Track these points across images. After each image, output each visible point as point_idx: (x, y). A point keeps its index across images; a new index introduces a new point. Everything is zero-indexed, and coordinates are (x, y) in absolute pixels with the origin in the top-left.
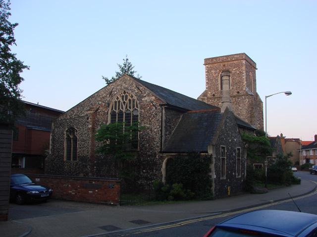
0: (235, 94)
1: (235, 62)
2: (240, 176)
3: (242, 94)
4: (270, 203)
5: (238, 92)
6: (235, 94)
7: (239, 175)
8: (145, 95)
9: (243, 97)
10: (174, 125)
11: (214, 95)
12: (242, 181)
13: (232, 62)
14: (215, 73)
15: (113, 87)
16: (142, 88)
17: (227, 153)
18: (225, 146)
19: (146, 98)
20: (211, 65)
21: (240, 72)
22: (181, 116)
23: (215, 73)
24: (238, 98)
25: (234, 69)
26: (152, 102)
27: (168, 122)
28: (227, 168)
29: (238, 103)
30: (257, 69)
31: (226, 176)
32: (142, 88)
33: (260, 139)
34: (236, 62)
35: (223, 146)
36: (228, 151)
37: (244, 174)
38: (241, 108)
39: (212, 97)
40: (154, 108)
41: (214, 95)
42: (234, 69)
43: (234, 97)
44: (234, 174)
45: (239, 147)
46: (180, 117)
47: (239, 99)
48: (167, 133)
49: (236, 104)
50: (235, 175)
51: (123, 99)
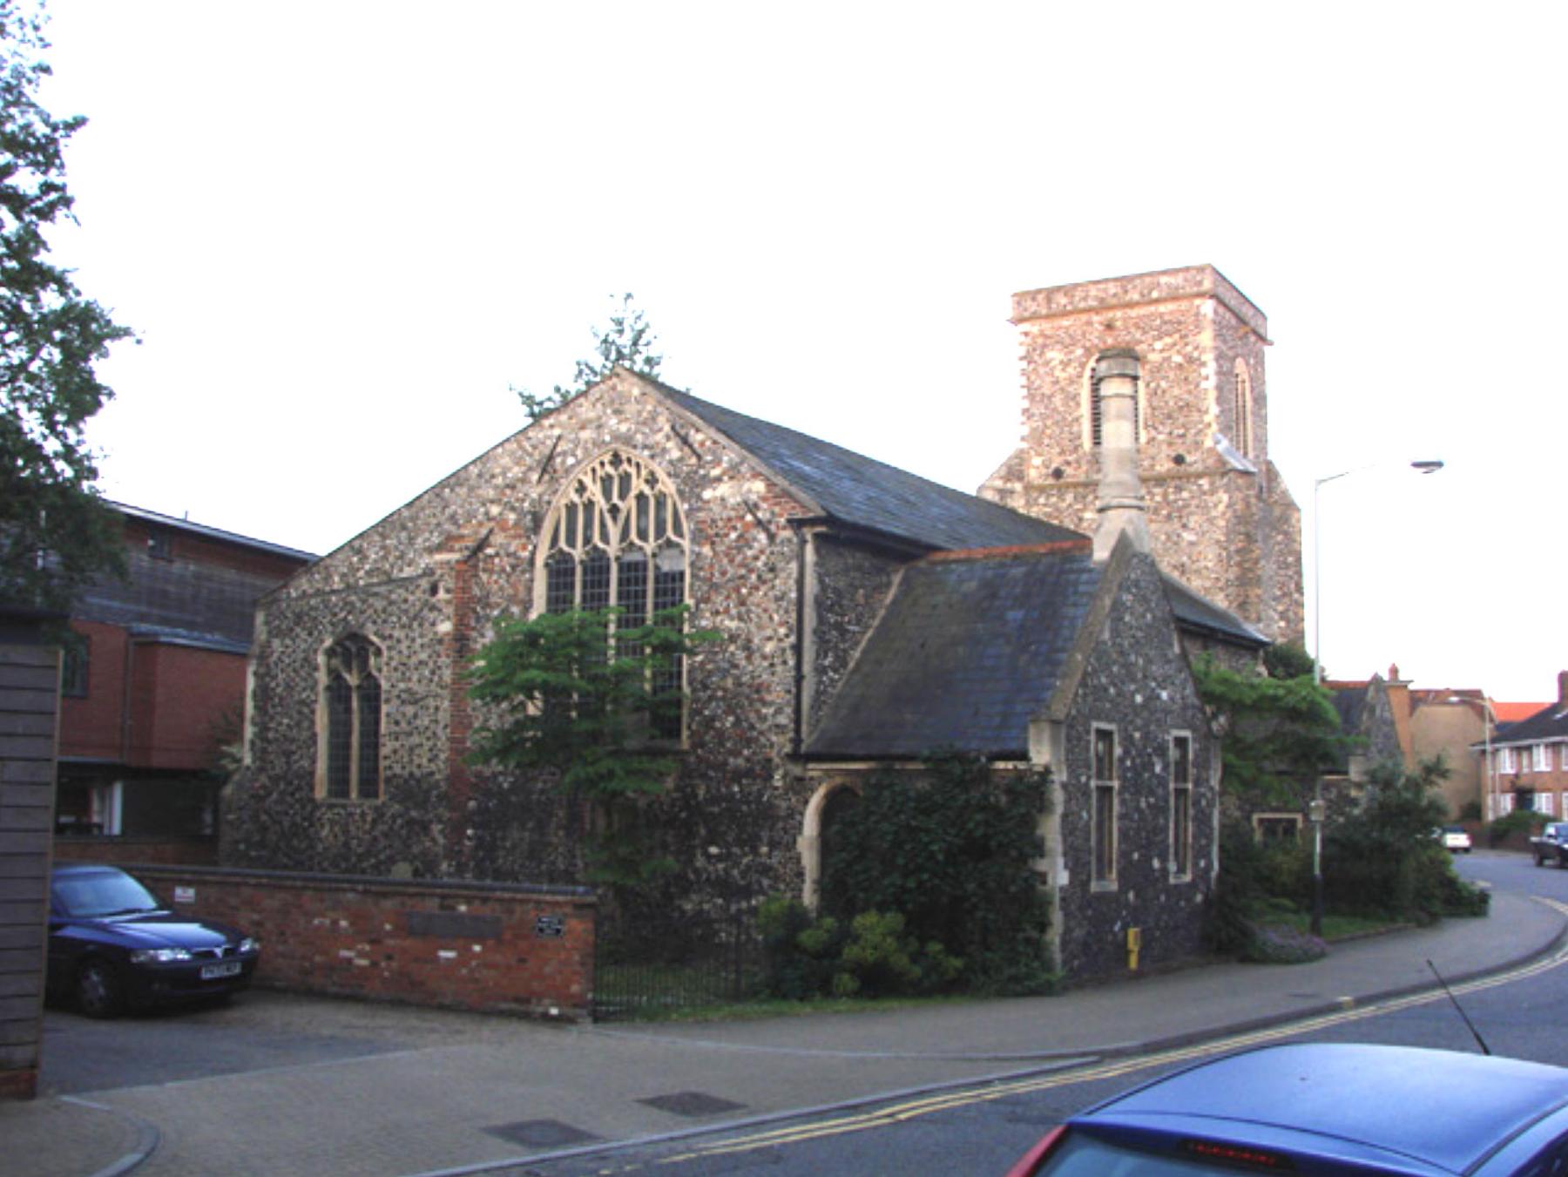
0: (1164, 466)
1: (1162, 308)
2: (1187, 878)
3: (1199, 467)
5: (1179, 460)
6: (1164, 466)
7: (1181, 870)
10: (858, 623)
11: (1058, 474)
17: (1122, 760)
22: (897, 579)
24: (1179, 489)
25: (1158, 345)
26: (753, 508)
28: (1124, 834)
29: (1177, 514)
32: (700, 437)
36: (1126, 752)
38: (1193, 538)
39: (1051, 481)
41: (1058, 474)
43: (1160, 481)
44: (1156, 864)
47: (1185, 495)
48: (826, 663)
49: (1169, 517)
50: (1164, 871)
51: (607, 493)
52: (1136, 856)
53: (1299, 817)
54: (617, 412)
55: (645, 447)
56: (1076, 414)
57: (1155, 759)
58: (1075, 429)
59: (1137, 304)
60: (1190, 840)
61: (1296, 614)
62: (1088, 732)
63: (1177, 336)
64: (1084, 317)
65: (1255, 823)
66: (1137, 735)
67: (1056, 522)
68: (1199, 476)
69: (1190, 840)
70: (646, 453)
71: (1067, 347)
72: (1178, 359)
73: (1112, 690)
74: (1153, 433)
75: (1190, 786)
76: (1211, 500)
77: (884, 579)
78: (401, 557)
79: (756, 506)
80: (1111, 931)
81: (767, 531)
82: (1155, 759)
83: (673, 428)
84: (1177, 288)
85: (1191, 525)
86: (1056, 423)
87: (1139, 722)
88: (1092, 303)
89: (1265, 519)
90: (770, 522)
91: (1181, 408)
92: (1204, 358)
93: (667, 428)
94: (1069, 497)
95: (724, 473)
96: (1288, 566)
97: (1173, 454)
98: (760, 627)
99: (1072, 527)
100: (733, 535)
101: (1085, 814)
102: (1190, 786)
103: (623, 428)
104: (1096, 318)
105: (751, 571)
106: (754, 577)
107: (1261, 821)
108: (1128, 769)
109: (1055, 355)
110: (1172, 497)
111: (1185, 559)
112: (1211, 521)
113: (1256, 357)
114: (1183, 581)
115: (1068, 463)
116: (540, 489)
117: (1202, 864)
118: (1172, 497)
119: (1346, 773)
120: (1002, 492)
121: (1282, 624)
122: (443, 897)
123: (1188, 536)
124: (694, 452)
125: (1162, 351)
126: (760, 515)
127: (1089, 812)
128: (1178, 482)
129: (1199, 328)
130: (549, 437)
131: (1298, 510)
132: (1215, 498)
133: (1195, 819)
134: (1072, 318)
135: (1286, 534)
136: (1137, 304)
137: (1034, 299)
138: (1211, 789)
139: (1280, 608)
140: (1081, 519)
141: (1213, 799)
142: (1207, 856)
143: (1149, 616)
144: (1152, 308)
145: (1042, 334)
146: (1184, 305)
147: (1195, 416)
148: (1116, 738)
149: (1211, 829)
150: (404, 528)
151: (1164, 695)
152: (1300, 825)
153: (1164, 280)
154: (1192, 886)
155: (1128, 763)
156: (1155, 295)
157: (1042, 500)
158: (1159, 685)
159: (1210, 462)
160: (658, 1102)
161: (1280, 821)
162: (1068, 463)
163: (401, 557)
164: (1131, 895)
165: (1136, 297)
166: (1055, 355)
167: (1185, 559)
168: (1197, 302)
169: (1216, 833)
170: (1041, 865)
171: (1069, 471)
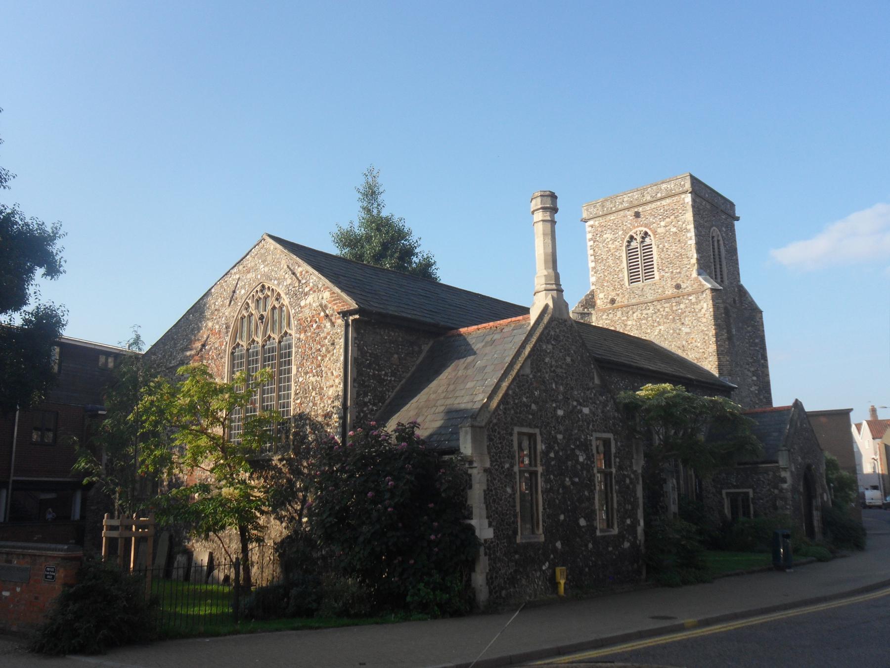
0: (670, 291)
1: (664, 202)
2: (615, 531)
3: (690, 289)
4: (681, 628)
5: (678, 287)
6: (670, 291)
7: (610, 525)
8: (307, 289)
9: (693, 298)
10: (393, 374)
11: (613, 301)
12: (627, 545)
13: (653, 205)
14: (614, 240)
15: (237, 276)
16: (300, 269)
17: (545, 454)
18: (537, 431)
19: (310, 299)
20: (601, 220)
21: (681, 230)
22: (426, 348)
23: (614, 240)
24: (679, 303)
25: (663, 224)
26: (323, 308)
27: (369, 366)
28: (549, 503)
29: (678, 318)
30: (738, 219)
31: (545, 532)
32: (300, 269)
33: (859, 426)
34: (668, 201)
35: (531, 431)
36: (550, 448)
37: (635, 523)
38: (688, 330)
39: (609, 306)
40: (328, 325)
41: (613, 301)
42: (663, 224)
43: (668, 299)
44: (582, 522)
45: (610, 436)
46: (420, 352)
47: (682, 306)
48: (366, 400)
49: (674, 320)
50: (592, 528)
51: (257, 307)
52: (562, 517)
53: (750, 491)
54: (264, 261)
55: (276, 279)
56: (621, 267)
57: (577, 452)
58: (620, 275)
59: (650, 202)
60: (615, 506)
61: (763, 372)
62: (511, 434)
63: (672, 217)
64: (622, 213)
65: (724, 496)
66: (560, 437)
67: (612, 328)
68: (689, 295)
69: (615, 506)
70: (276, 282)
71: (614, 231)
72: (674, 230)
73: (534, 407)
74: (663, 273)
75: (614, 470)
76: (698, 307)
77: (416, 349)
78: (171, 356)
79: (326, 306)
80: (541, 570)
81: (331, 320)
82: (577, 452)
83: (288, 267)
84: (671, 190)
85: (687, 322)
86: (610, 274)
87: (562, 428)
88: (626, 205)
89: (739, 320)
90: (332, 315)
91: (678, 257)
92: (688, 227)
93: (286, 267)
94: (619, 314)
95: (311, 290)
96: (756, 345)
97: (674, 284)
98: (327, 379)
99: (621, 331)
100: (315, 326)
101: (509, 490)
102: (614, 470)
103: (266, 269)
104: (628, 213)
105: (322, 346)
106: (324, 349)
107: (727, 494)
108: (553, 459)
109: (608, 236)
110: (674, 308)
111: (684, 343)
112: (698, 319)
113: (727, 227)
114: (684, 355)
115: (618, 295)
116: (229, 310)
117: (628, 521)
118: (674, 308)
119: (777, 462)
120: (583, 315)
121: (755, 378)
122: (7, 554)
123: (685, 330)
124: (298, 279)
125: (665, 226)
126: (327, 312)
127: (513, 488)
128: (678, 299)
129: (685, 210)
130: (234, 280)
131: (761, 312)
132: (699, 307)
133: (619, 492)
134: (615, 215)
135: (753, 326)
136: (650, 202)
137: (595, 207)
138: (635, 472)
139: (752, 369)
140: (625, 325)
141: (637, 479)
142: (633, 515)
143: (568, 359)
144: (658, 203)
145: (601, 226)
146: (675, 199)
147: (685, 261)
148: (539, 438)
149: (636, 499)
150: (173, 339)
151: (586, 410)
152: (751, 495)
153: (664, 186)
154: (621, 537)
155: (552, 455)
156: (659, 195)
157: (604, 317)
158: (580, 404)
159: (695, 286)
160: (653, 618)
161: (739, 493)
162: (618, 295)
163: (171, 356)
164: (559, 545)
165: (649, 198)
166: (608, 236)
167: (684, 343)
168: (683, 196)
169: (641, 501)
170: (473, 522)
171: (618, 299)
